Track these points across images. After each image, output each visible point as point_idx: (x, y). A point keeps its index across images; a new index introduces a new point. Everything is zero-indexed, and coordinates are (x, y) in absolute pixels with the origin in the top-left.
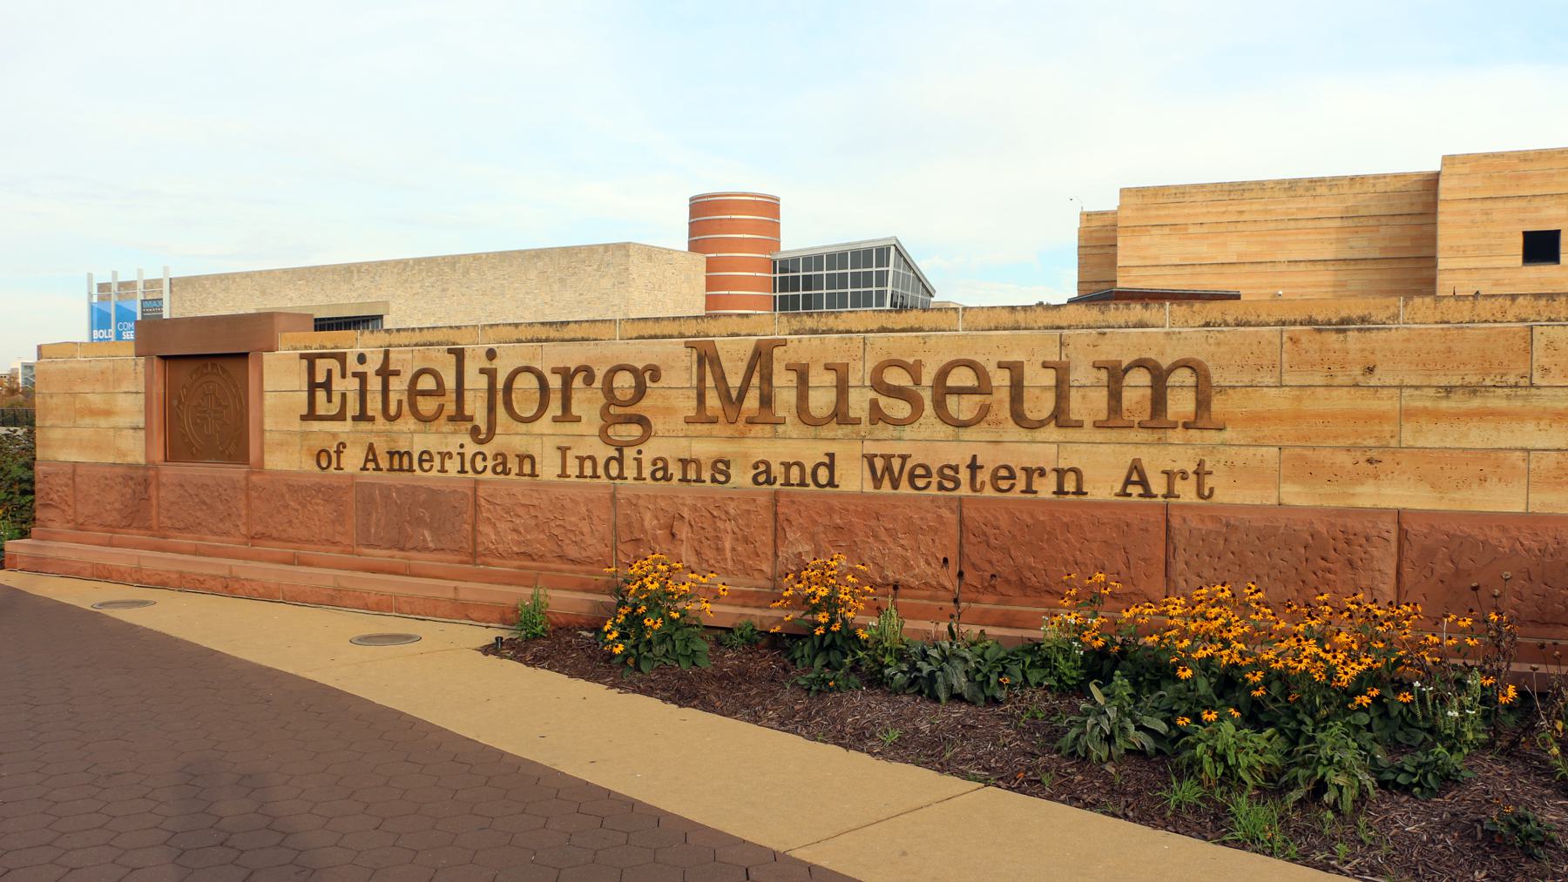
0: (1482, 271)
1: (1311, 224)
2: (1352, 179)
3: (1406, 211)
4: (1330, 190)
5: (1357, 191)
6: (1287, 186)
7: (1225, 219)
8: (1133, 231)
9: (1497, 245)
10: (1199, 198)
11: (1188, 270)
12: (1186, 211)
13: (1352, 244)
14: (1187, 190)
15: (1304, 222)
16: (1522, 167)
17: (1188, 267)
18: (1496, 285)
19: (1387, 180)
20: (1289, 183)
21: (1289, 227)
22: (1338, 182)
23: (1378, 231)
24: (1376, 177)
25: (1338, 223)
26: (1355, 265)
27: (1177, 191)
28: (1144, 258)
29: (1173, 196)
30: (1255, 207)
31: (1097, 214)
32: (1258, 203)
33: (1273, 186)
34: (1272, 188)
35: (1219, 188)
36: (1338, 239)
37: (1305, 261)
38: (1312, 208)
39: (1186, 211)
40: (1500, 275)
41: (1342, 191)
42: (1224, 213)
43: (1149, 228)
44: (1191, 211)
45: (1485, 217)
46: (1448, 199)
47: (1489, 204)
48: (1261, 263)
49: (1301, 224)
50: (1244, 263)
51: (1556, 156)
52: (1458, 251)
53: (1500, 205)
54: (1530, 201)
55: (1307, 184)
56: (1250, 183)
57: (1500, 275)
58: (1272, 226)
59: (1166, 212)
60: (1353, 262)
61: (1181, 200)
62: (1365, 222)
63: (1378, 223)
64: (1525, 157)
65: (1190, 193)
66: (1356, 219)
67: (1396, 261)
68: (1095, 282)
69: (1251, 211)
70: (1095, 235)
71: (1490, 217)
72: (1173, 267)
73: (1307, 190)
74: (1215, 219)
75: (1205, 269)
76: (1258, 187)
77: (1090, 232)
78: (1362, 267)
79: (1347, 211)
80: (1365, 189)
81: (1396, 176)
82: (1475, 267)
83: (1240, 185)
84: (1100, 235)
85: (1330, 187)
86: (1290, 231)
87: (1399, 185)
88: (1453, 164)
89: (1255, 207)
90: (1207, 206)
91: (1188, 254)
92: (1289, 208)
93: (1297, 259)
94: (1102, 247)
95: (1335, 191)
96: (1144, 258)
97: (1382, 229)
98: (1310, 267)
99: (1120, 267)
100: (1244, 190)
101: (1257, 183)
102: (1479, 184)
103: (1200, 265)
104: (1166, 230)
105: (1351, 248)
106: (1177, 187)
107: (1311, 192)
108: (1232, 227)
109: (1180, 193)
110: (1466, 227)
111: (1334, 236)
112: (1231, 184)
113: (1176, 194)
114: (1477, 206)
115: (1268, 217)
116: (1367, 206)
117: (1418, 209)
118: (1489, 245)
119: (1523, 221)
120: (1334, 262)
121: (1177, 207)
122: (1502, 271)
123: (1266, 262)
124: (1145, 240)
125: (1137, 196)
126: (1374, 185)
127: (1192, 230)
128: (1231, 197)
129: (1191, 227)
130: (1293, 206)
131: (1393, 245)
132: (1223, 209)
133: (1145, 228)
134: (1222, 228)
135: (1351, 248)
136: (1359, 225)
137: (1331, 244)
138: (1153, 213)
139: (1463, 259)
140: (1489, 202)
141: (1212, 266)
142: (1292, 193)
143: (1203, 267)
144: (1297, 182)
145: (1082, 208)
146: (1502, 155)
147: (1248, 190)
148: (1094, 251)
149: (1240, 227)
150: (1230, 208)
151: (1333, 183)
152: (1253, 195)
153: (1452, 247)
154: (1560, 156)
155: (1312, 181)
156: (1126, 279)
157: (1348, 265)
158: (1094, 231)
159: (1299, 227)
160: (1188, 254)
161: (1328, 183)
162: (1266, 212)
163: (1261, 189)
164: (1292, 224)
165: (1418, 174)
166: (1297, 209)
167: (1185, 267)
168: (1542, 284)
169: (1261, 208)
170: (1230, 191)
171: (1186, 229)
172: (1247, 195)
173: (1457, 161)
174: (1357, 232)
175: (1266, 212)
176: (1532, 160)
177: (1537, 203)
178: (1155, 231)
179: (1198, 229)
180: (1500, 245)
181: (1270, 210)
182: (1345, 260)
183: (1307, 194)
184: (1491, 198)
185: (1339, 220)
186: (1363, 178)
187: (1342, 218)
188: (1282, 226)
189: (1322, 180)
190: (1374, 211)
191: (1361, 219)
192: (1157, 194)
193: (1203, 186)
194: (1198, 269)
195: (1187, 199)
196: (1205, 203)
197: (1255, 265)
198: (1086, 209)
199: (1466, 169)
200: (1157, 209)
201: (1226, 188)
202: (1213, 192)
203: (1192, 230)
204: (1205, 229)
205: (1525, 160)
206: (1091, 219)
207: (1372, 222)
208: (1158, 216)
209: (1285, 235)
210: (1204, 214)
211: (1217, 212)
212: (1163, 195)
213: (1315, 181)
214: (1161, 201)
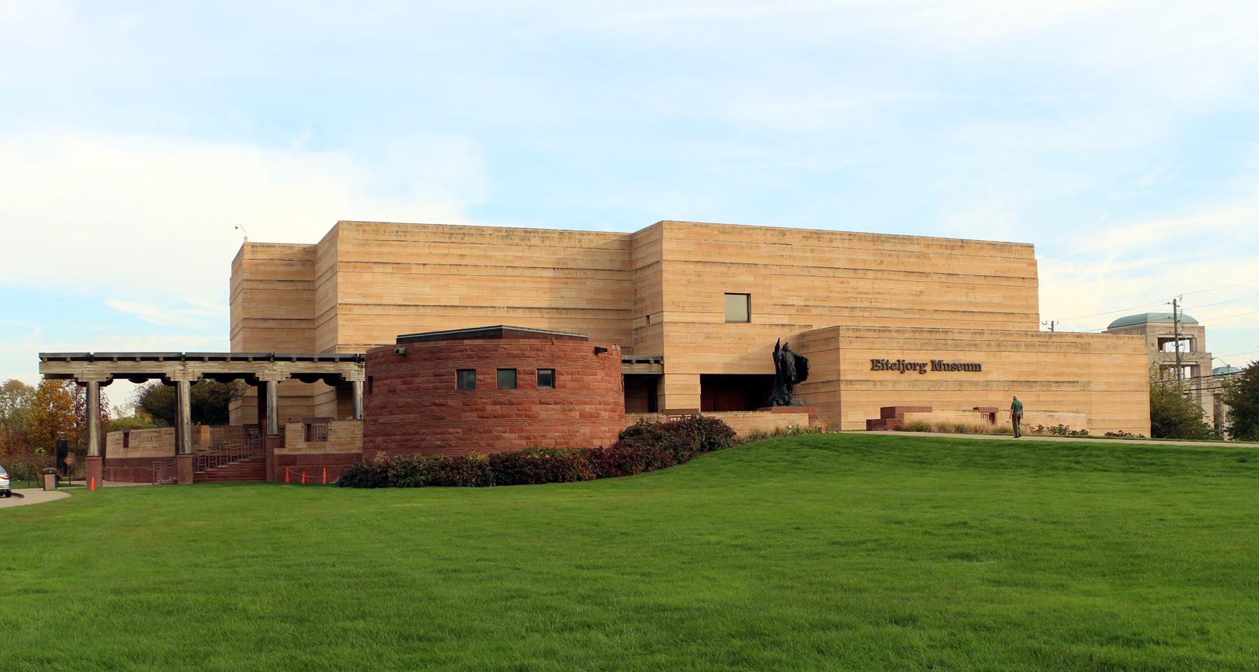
0: (697, 325)
1: (527, 272)
2: (562, 233)
3: (608, 266)
4: (543, 242)
5: (565, 245)
6: (504, 234)
7: (448, 261)
8: (355, 267)
9: (707, 303)
10: (421, 238)
11: (412, 311)
12: (409, 250)
13: (563, 294)
14: (409, 229)
15: (521, 270)
16: (722, 237)
17: (411, 308)
18: (707, 338)
19: (591, 237)
20: (506, 232)
21: (507, 274)
22: (549, 235)
23: (585, 283)
24: (582, 233)
25: (551, 273)
26: (566, 313)
27: (399, 229)
28: (366, 296)
29: (395, 233)
30: (476, 252)
31: (263, 246)
32: (478, 248)
33: (491, 232)
34: (491, 235)
35: (440, 230)
36: (551, 288)
37: (522, 308)
38: (528, 257)
39: (409, 250)
40: (710, 329)
41: (553, 243)
42: (446, 255)
43: (371, 265)
44: (414, 251)
45: (697, 278)
46: (669, 259)
47: (699, 267)
48: (483, 307)
49: (518, 272)
50: (467, 307)
51: (744, 231)
52: (679, 306)
53: (708, 268)
54: (729, 267)
55: (523, 234)
56: (470, 228)
57: (710, 329)
58: (492, 271)
59: (388, 250)
60: (564, 311)
61: (403, 238)
62: (573, 274)
63: (585, 276)
64: (724, 230)
65: (411, 232)
66: (566, 271)
67: (601, 312)
68: (263, 319)
69: (471, 256)
70: (261, 268)
71: (701, 278)
72: (396, 307)
73: (523, 239)
74: (437, 261)
75: (428, 311)
76: (478, 232)
77: (257, 265)
78: (572, 316)
79: (558, 263)
80: (572, 243)
81: (597, 234)
82: (691, 321)
83: (460, 229)
84: (268, 268)
85: (543, 239)
86: (509, 278)
87: (601, 242)
88: (672, 229)
89: (476, 252)
90: (429, 247)
91: (411, 294)
92: (507, 256)
93: (516, 306)
94: (269, 281)
95: (547, 243)
96: (366, 296)
97: (588, 282)
98: (527, 314)
99: (340, 304)
100: (464, 234)
101: (477, 228)
102: (692, 249)
103: (424, 306)
104: (389, 269)
105: (562, 297)
106: (398, 225)
107: (526, 242)
108: (454, 270)
109: (402, 232)
110: (684, 286)
111: (547, 286)
112: (452, 227)
113: (397, 232)
114: (692, 267)
115: (488, 263)
116: (575, 260)
117: (616, 266)
118: (701, 303)
119: (725, 284)
120: (548, 310)
121: (400, 245)
122: (711, 326)
123: (487, 307)
124: (367, 277)
125: (358, 230)
126: (580, 241)
127: (415, 270)
128: (453, 240)
129: (413, 266)
130: (512, 253)
131: (597, 297)
132: (446, 251)
133: (368, 265)
134: (445, 271)
135: (562, 297)
136: (569, 276)
137: (545, 293)
138: (374, 249)
139: (682, 314)
140: (700, 265)
141: (435, 308)
142: (509, 242)
143: (426, 308)
144: (513, 231)
145: (246, 238)
146: (707, 226)
147: (469, 234)
148: (261, 286)
149: (462, 270)
150: (451, 251)
151: (544, 234)
152: (474, 240)
153: (674, 302)
154: (747, 232)
155: (526, 231)
156: (347, 317)
157: (560, 313)
158: (260, 264)
159: (516, 274)
160: (411, 294)
161: (540, 235)
162: (486, 257)
163: (480, 234)
164: (510, 271)
165: (615, 234)
166: (514, 256)
167: (408, 308)
168: (740, 339)
169: (482, 253)
170: (451, 234)
171: (410, 269)
172: (467, 239)
173: (674, 227)
174: (567, 283)
175: (486, 257)
176: (728, 233)
177: (733, 269)
178: (377, 269)
179: (421, 270)
180: (709, 303)
181: (490, 256)
182: (557, 309)
183: (523, 243)
184: (701, 262)
185: (552, 270)
186: (570, 233)
187: (554, 268)
188: (500, 272)
189: (536, 231)
190: (581, 265)
191: (571, 272)
192: (378, 230)
193: (424, 226)
194: (422, 310)
195: (409, 238)
196: (427, 244)
197: (477, 310)
198: (251, 240)
199: (681, 235)
200: (379, 246)
201: (447, 230)
202: (435, 233)
203: (415, 270)
204: (428, 270)
205: (723, 232)
206: (256, 251)
207: (580, 274)
208: (381, 254)
209: (504, 281)
210: (427, 255)
211: (439, 254)
212: (384, 232)
213: (529, 232)
214: (383, 238)
